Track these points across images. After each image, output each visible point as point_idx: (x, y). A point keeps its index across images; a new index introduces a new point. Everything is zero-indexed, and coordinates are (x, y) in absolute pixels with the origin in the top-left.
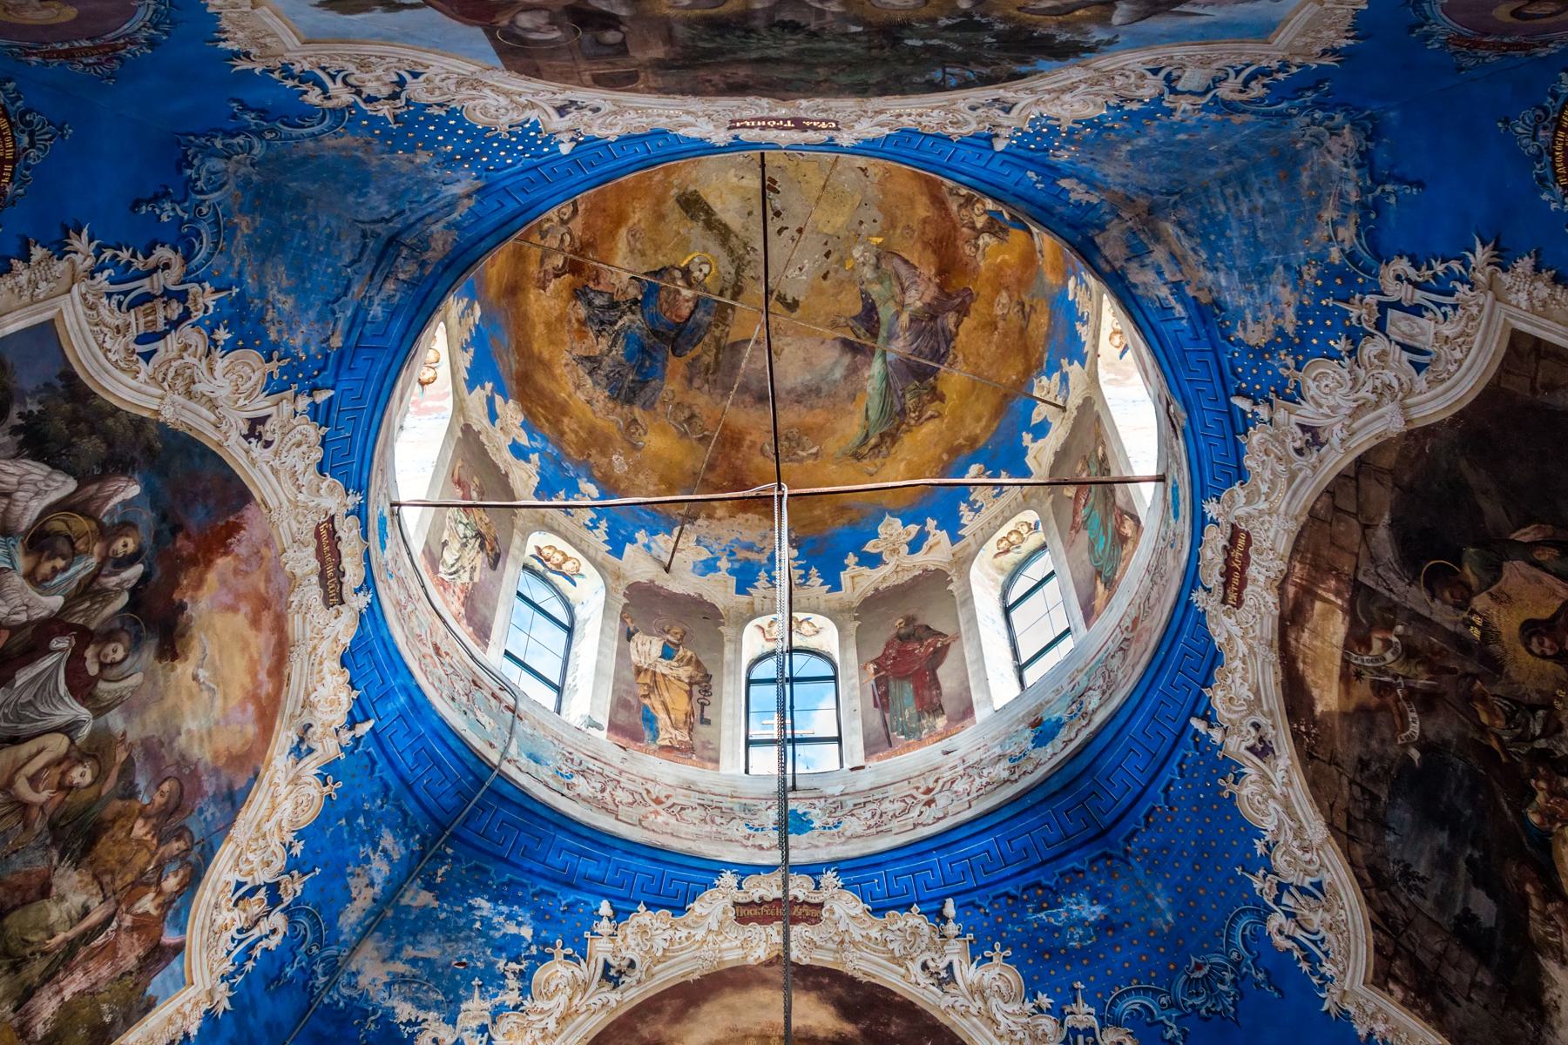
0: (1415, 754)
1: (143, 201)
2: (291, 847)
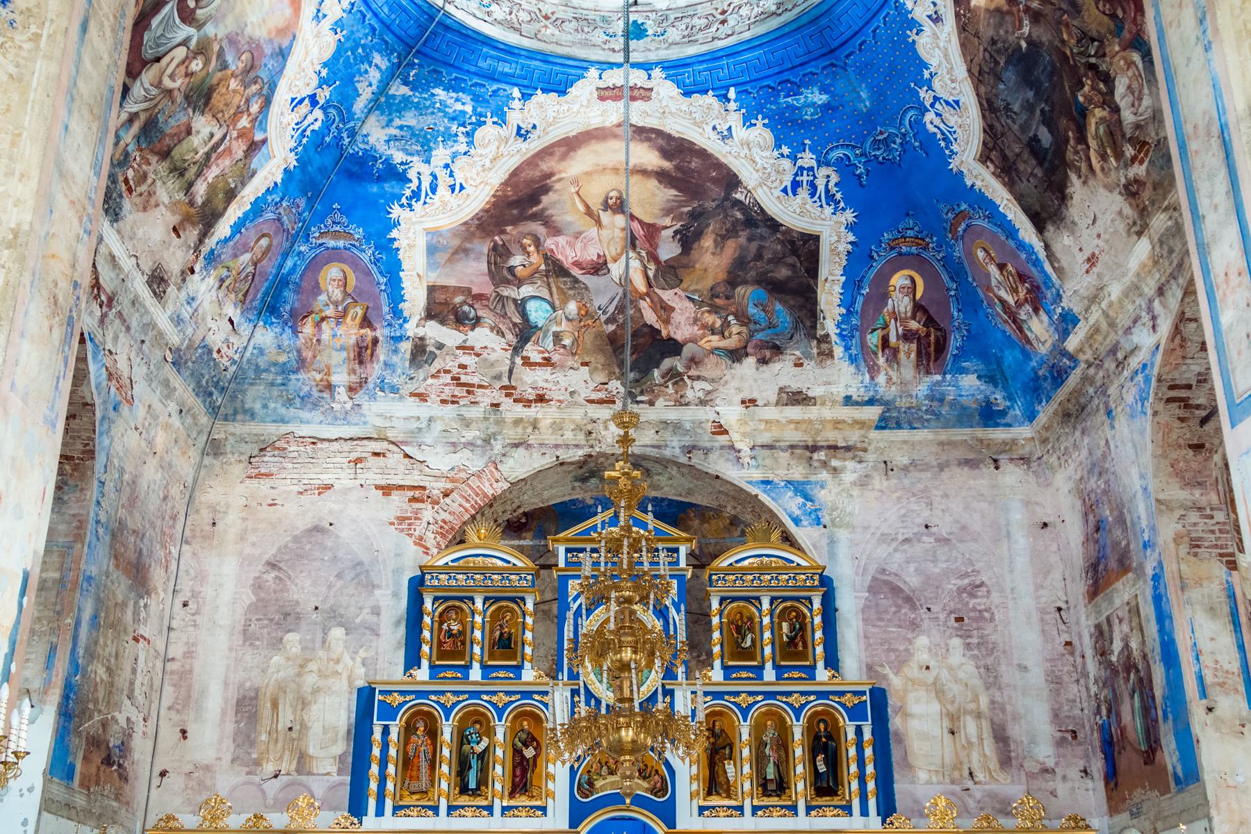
0: (1024, 45)
2: (782, 155)
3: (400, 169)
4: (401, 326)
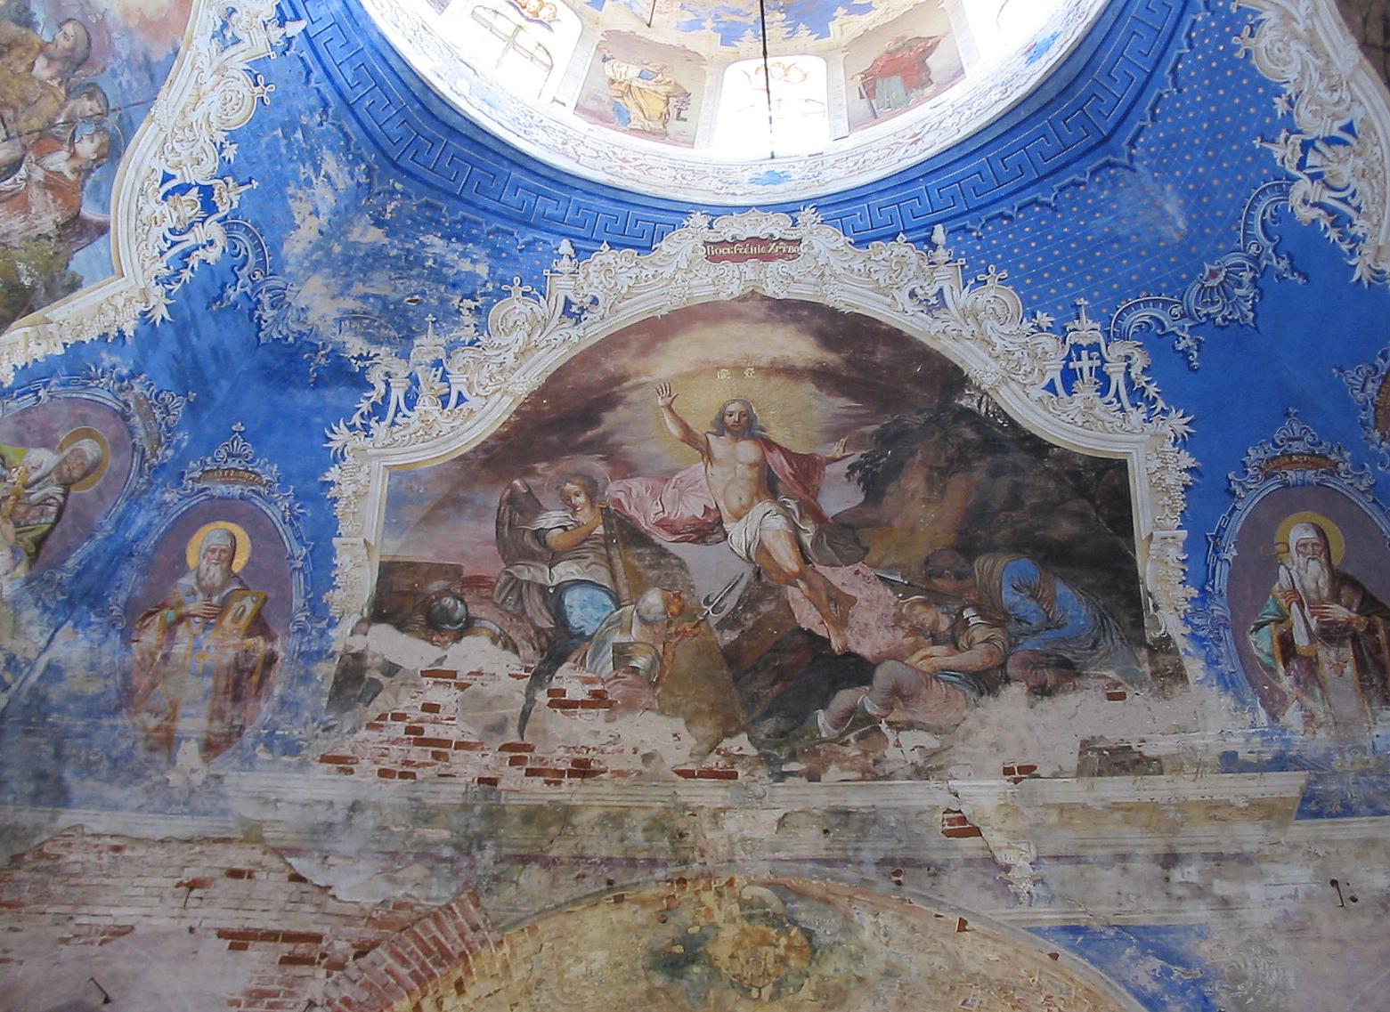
3: (357, 366)
4: (322, 633)
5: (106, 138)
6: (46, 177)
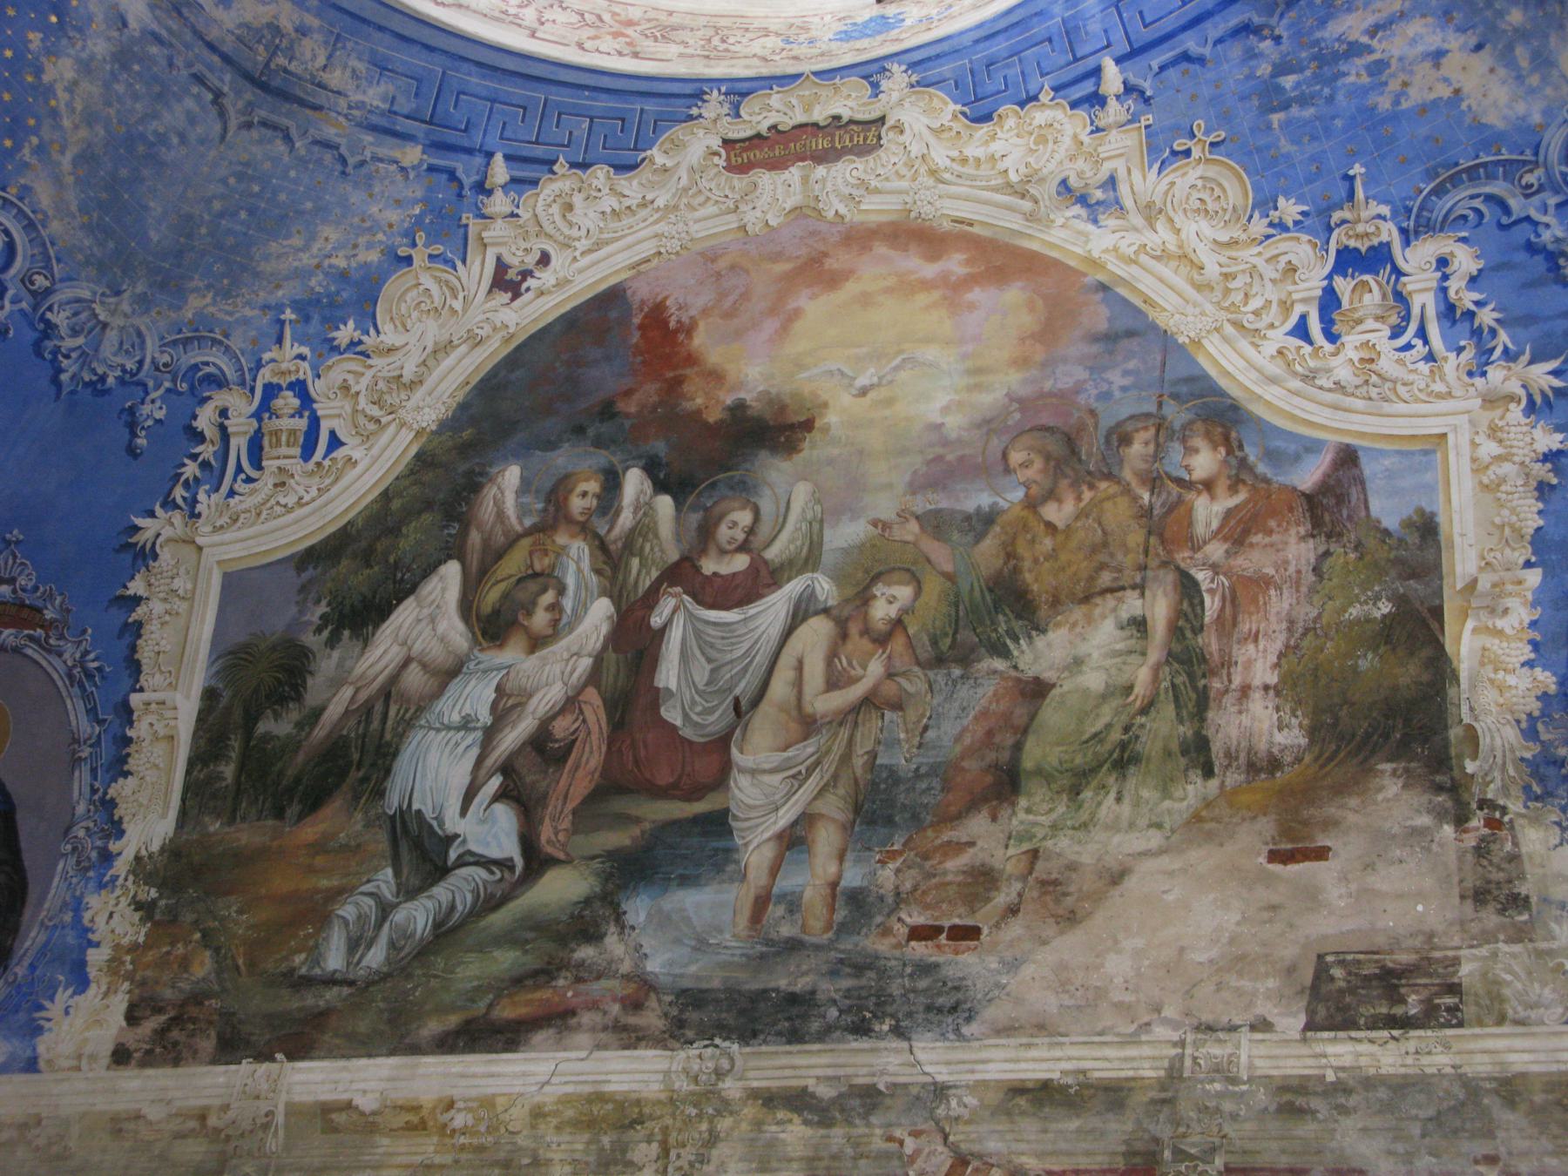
1: (131, 442)
2: (1281, 226)
5: (1199, 426)
6: (1225, 539)
